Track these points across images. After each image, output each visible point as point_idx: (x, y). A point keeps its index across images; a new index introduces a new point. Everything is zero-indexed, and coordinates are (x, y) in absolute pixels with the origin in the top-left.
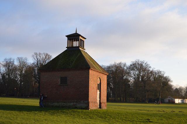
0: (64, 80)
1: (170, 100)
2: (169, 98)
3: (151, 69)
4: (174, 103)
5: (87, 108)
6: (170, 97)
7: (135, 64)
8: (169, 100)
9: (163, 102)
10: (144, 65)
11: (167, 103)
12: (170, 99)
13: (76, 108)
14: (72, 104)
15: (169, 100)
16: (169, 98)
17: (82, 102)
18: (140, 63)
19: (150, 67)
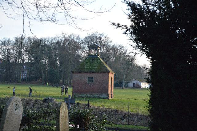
0: (90, 80)
1: (135, 83)
2: (134, 82)
3: (112, 44)
4: (139, 87)
5: (107, 98)
6: (135, 81)
7: (92, 37)
8: (134, 84)
9: (127, 87)
10: (103, 38)
11: (131, 88)
12: (135, 82)
13: (100, 98)
14: (97, 95)
15: (134, 84)
16: (134, 82)
17: (104, 94)
18: (98, 36)
19: (111, 42)
